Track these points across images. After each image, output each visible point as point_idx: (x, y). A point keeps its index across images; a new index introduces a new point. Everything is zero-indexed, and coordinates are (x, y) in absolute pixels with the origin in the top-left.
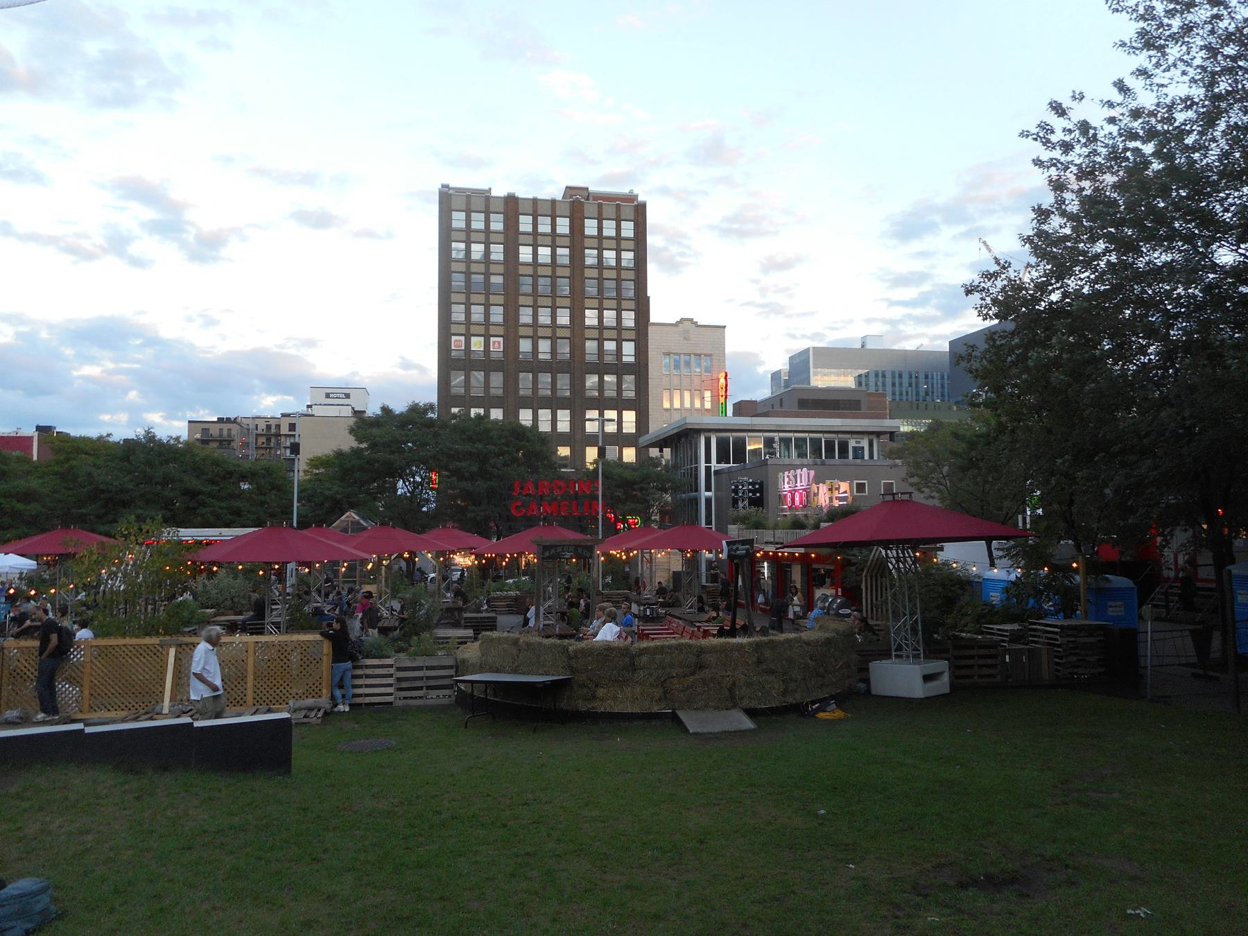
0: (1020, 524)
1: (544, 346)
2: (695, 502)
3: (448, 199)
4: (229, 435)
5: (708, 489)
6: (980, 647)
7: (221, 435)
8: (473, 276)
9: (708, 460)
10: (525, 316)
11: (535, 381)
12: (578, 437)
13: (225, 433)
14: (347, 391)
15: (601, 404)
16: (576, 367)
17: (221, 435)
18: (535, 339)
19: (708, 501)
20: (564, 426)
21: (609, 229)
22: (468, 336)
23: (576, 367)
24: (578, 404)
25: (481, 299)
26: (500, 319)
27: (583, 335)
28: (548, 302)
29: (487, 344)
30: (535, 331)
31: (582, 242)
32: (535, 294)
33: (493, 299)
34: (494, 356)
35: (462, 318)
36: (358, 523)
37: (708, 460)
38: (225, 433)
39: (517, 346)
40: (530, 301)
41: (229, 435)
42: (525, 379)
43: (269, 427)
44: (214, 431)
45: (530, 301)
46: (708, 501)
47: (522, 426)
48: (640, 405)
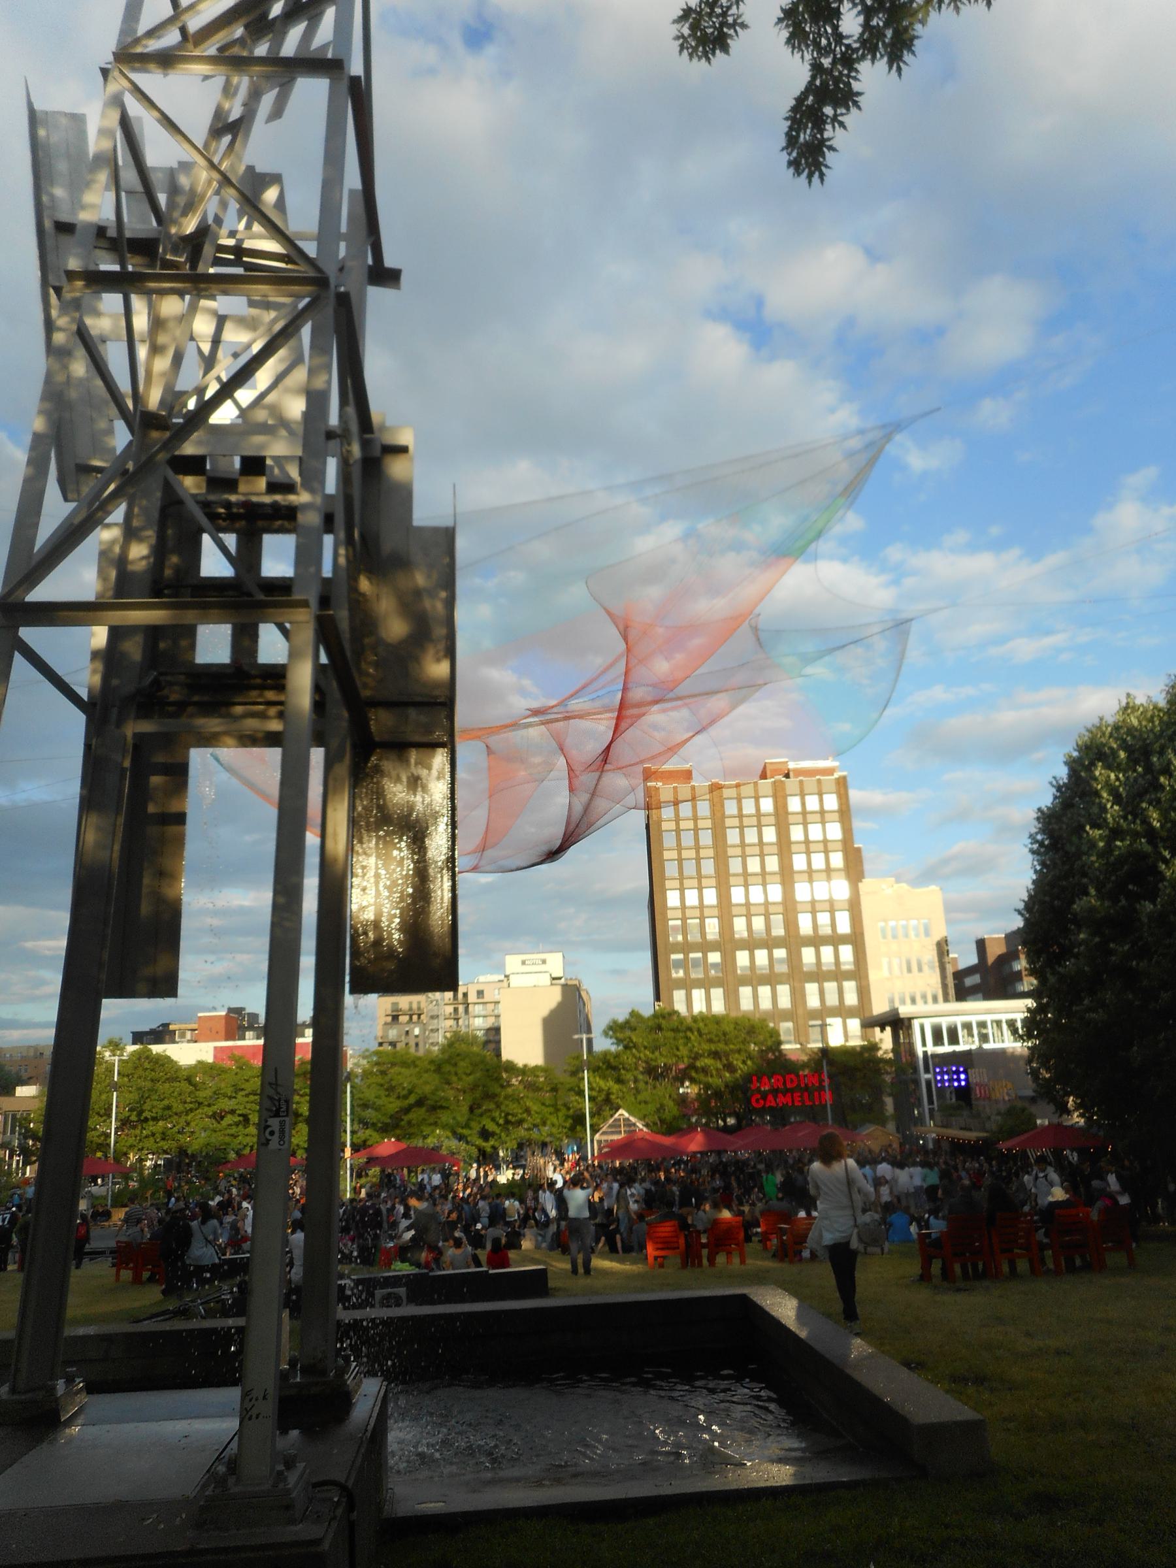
1: (758, 923)
2: (917, 1082)
3: (399, 288)
4: (419, 1008)
5: (927, 1071)
6: (517, 1480)
7: (411, 1009)
8: (710, 937)
9: (924, 1044)
11: (752, 958)
12: (800, 1011)
13: (415, 1006)
15: (819, 975)
16: (728, 944)
17: (411, 1009)
18: (749, 917)
19: (928, 1083)
20: (785, 1002)
21: (812, 803)
22: (749, 917)
23: (728, 944)
24: (797, 976)
31: (787, 818)
34: (710, 937)
36: (628, 1119)
37: (924, 1044)
38: (415, 1006)
41: (419, 1008)
42: (742, 958)
46: (928, 1083)
48: (859, 973)
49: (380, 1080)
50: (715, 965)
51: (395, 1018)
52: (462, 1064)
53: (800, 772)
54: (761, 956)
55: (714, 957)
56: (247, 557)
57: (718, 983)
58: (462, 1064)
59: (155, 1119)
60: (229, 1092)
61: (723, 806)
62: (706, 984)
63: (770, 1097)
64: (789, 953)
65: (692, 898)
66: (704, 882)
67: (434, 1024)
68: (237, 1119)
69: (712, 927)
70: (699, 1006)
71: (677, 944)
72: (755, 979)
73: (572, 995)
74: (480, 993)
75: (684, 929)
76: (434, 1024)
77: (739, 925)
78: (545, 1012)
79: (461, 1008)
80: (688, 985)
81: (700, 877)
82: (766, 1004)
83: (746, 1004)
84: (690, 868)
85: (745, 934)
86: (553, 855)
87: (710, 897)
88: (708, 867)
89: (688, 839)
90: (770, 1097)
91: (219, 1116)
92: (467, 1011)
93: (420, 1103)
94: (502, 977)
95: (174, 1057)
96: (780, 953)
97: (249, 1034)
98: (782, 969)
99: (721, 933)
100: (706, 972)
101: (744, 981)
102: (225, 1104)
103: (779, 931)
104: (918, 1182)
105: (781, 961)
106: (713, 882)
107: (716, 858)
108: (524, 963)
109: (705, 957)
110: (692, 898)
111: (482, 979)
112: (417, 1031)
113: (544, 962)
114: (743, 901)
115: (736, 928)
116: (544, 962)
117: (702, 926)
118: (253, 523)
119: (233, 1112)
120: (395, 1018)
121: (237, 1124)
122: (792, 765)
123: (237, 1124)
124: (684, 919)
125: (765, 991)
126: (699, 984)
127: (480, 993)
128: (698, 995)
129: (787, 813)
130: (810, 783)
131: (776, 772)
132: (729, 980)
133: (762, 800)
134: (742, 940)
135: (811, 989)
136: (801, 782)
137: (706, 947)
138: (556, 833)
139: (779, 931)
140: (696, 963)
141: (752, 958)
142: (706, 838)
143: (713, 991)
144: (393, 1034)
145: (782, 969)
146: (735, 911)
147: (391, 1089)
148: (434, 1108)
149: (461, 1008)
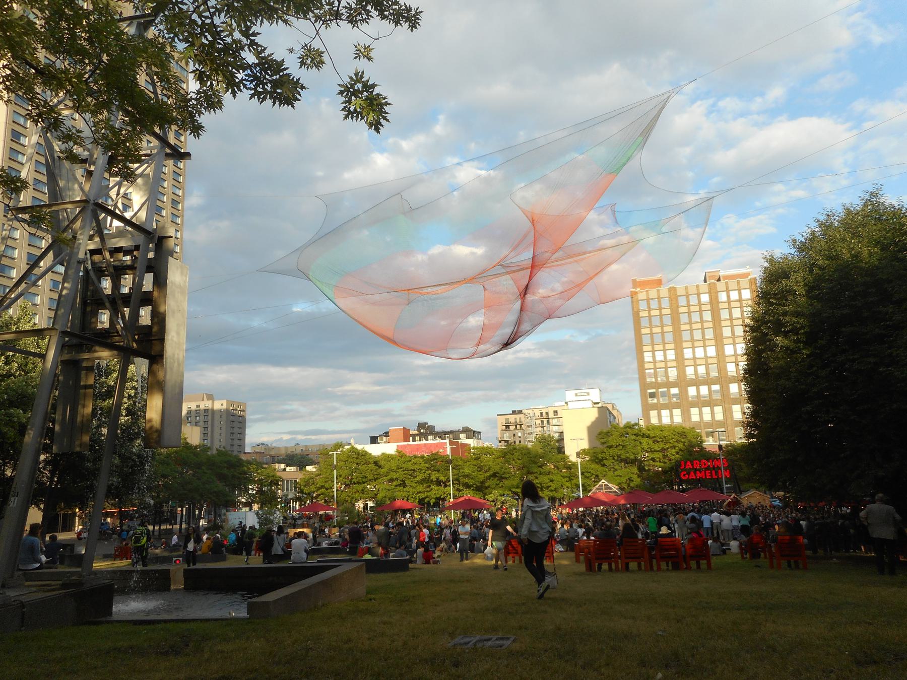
0: (643, 563)
1: (702, 370)
2: (57, 516)
8: (671, 379)
10: (688, 353)
11: (698, 391)
12: (729, 422)
13: (518, 421)
14: (578, 398)
16: (683, 383)
18: (695, 366)
20: (719, 416)
22: (695, 366)
25: (661, 347)
26: (673, 357)
27: (724, 361)
28: (701, 343)
29: (696, 371)
30: (695, 362)
32: (692, 340)
33: (668, 347)
34: (671, 379)
35: (651, 359)
38: (518, 421)
39: (684, 371)
40: (690, 344)
42: (692, 391)
43: (542, 414)
44: (512, 419)
45: (690, 344)
47: (187, 446)
49: (475, 463)
50: (674, 395)
51: (507, 427)
52: (516, 454)
53: (726, 277)
54: (704, 390)
55: (675, 391)
56: (116, 286)
57: (677, 406)
58: (516, 454)
59: (358, 483)
60: (395, 468)
61: (677, 300)
62: (670, 407)
63: (692, 473)
64: (722, 387)
65: (659, 356)
66: (707, 343)
67: (530, 430)
68: (399, 482)
69: (673, 373)
70: (666, 420)
71: (651, 383)
72: (700, 403)
73: (605, 412)
74: (556, 412)
75: (656, 375)
76: (530, 430)
77: (690, 371)
78: (589, 423)
79: (545, 421)
80: (659, 408)
81: (704, 339)
82: (695, 418)
83: (695, 418)
84: (698, 335)
85: (693, 377)
86: (506, 345)
87: (671, 355)
88: (709, 334)
89: (696, 317)
90: (692, 473)
91: (391, 480)
92: (548, 422)
93: (494, 475)
94: (563, 403)
95: (369, 451)
96: (716, 387)
97: (430, 437)
98: (717, 397)
99: (678, 376)
100: (670, 399)
101: (694, 405)
102: (394, 475)
103: (714, 374)
104: (735, 523)
105: (716, 392)
106: (713, 342)
107: (714, 328)
108: (576, 395)
109: (669, 391)
110: (659, 356)
111: (556, 404)
112: (520, 434)
113: (588, 394)
114: (691, 356)
115: (688, 373)
116: (588, 394)
117: (666, 372)
118: (118, 272)
119: (397, 479)
120: (507, 427)
121: (399, 485)
122: (722, 273)
123: (399, 485)
124: (655, 368)
125: (706, 410)
126: (665, 406)
127: (556, 412)
128: (665, 413)
129: (718, 302)
130: (733, 284)
131: (712, 277)
132: (685, 404)
133: (731, 293)
134: (692, 380)
135: (694, 411)
136: (727, 283)
137: (669, 384)
138: (507, 331)
139: (714, 374)
140: (663, 394)
141: (698, 391)
142: (707, 316)
143: (715, 408)
144: (506, 436)
145: (717, 397)
146: (728, 359)
147: (480, 468)
148: (501, 478)
149: (545, 421)
